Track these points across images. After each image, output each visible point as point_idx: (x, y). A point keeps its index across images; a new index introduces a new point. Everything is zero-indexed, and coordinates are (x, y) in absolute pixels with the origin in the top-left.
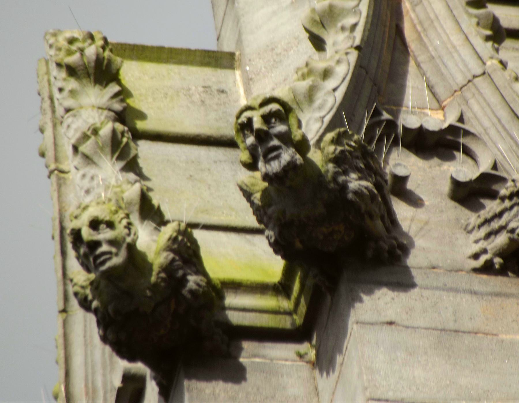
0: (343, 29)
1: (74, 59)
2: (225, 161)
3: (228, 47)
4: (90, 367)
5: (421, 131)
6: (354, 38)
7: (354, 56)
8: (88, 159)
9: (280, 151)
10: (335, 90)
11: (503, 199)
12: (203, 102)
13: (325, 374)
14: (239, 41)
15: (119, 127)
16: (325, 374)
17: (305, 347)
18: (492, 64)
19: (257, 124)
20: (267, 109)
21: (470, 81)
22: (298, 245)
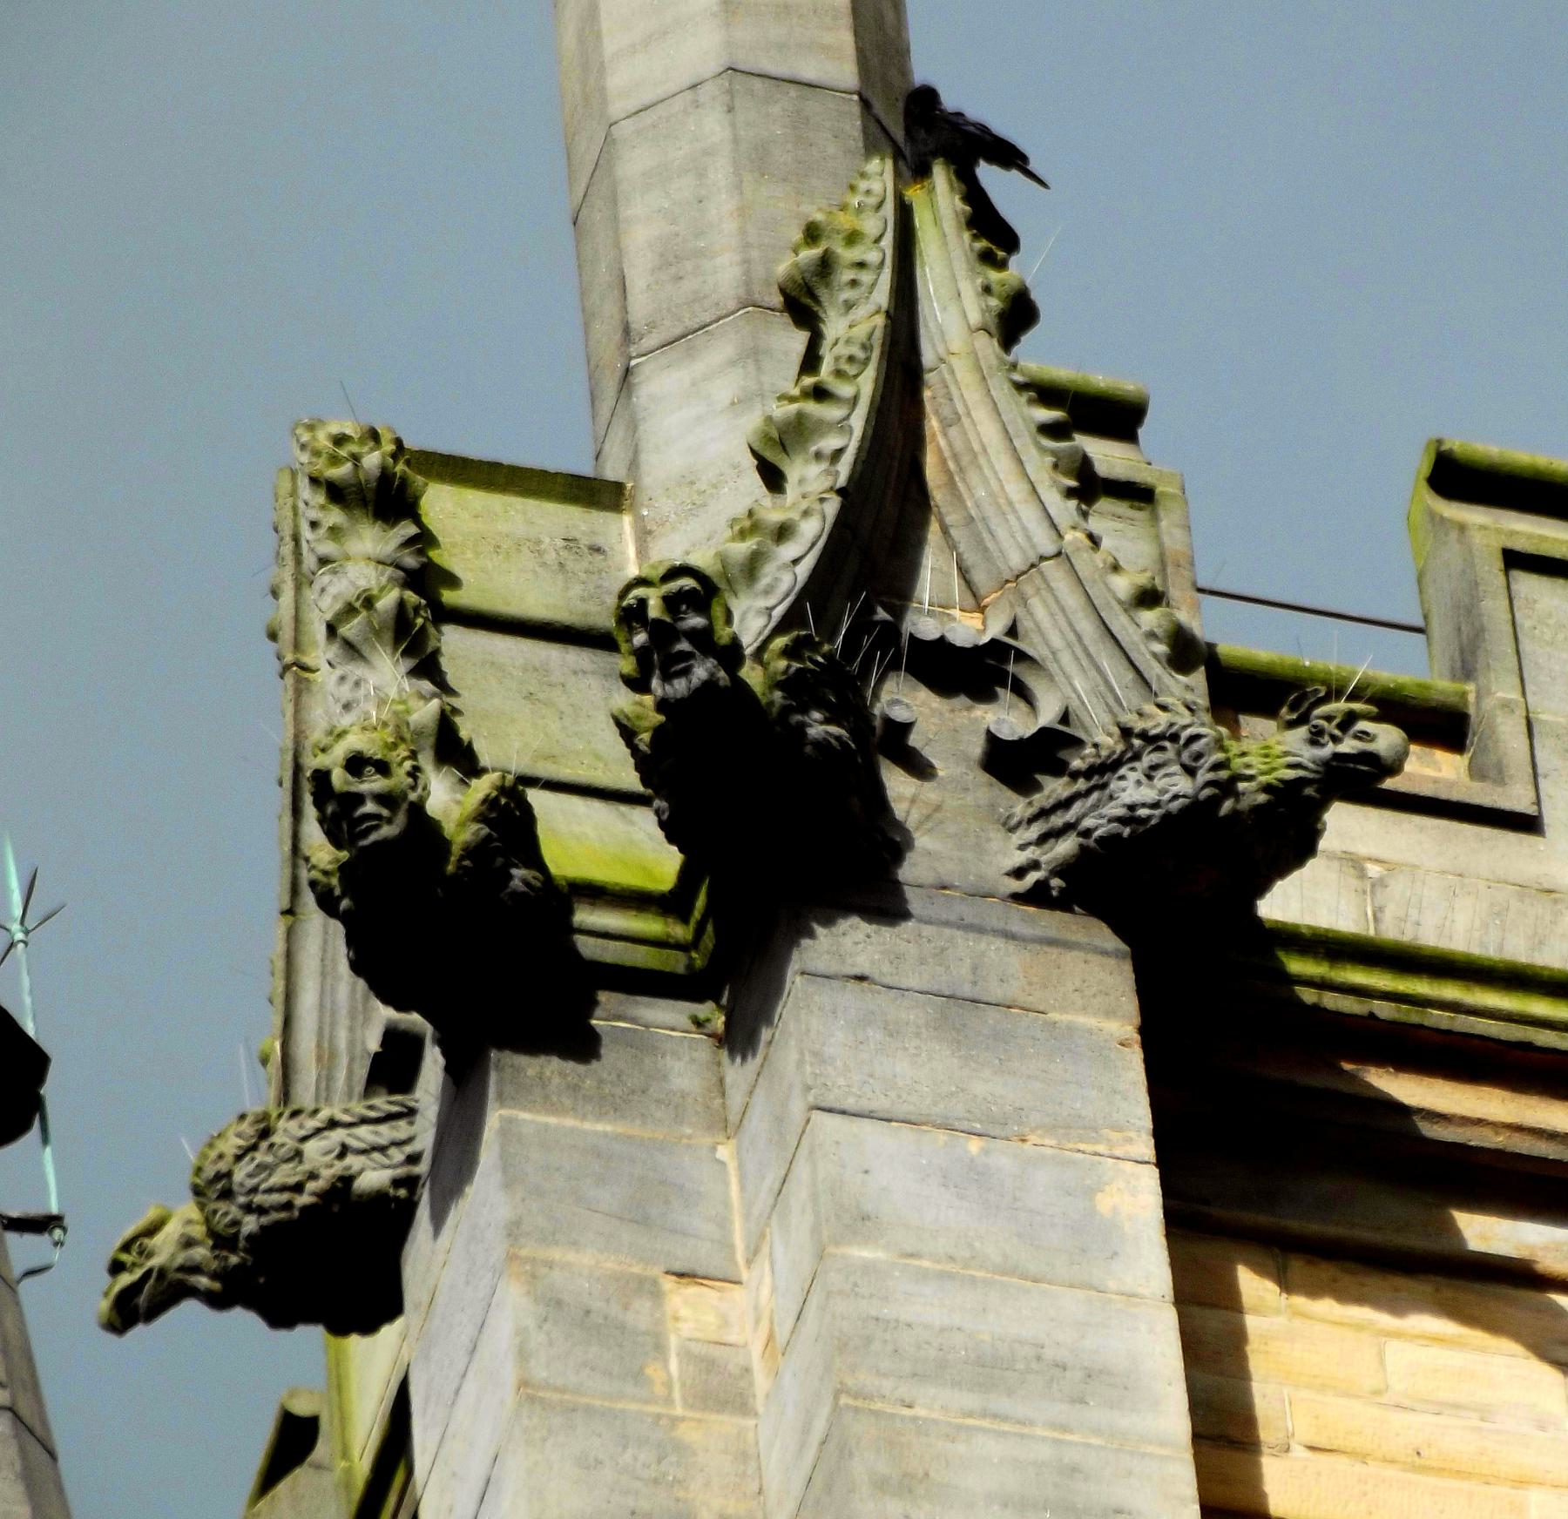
1: (341, 472)
3: (613, 470)
7: (833, 506)
10: (796, 562)
11: (1075, 775)
14: (634, 465)
15: (412, 597)
17: (705, 1009)
19: (655, 610)
21: (1033, 566)
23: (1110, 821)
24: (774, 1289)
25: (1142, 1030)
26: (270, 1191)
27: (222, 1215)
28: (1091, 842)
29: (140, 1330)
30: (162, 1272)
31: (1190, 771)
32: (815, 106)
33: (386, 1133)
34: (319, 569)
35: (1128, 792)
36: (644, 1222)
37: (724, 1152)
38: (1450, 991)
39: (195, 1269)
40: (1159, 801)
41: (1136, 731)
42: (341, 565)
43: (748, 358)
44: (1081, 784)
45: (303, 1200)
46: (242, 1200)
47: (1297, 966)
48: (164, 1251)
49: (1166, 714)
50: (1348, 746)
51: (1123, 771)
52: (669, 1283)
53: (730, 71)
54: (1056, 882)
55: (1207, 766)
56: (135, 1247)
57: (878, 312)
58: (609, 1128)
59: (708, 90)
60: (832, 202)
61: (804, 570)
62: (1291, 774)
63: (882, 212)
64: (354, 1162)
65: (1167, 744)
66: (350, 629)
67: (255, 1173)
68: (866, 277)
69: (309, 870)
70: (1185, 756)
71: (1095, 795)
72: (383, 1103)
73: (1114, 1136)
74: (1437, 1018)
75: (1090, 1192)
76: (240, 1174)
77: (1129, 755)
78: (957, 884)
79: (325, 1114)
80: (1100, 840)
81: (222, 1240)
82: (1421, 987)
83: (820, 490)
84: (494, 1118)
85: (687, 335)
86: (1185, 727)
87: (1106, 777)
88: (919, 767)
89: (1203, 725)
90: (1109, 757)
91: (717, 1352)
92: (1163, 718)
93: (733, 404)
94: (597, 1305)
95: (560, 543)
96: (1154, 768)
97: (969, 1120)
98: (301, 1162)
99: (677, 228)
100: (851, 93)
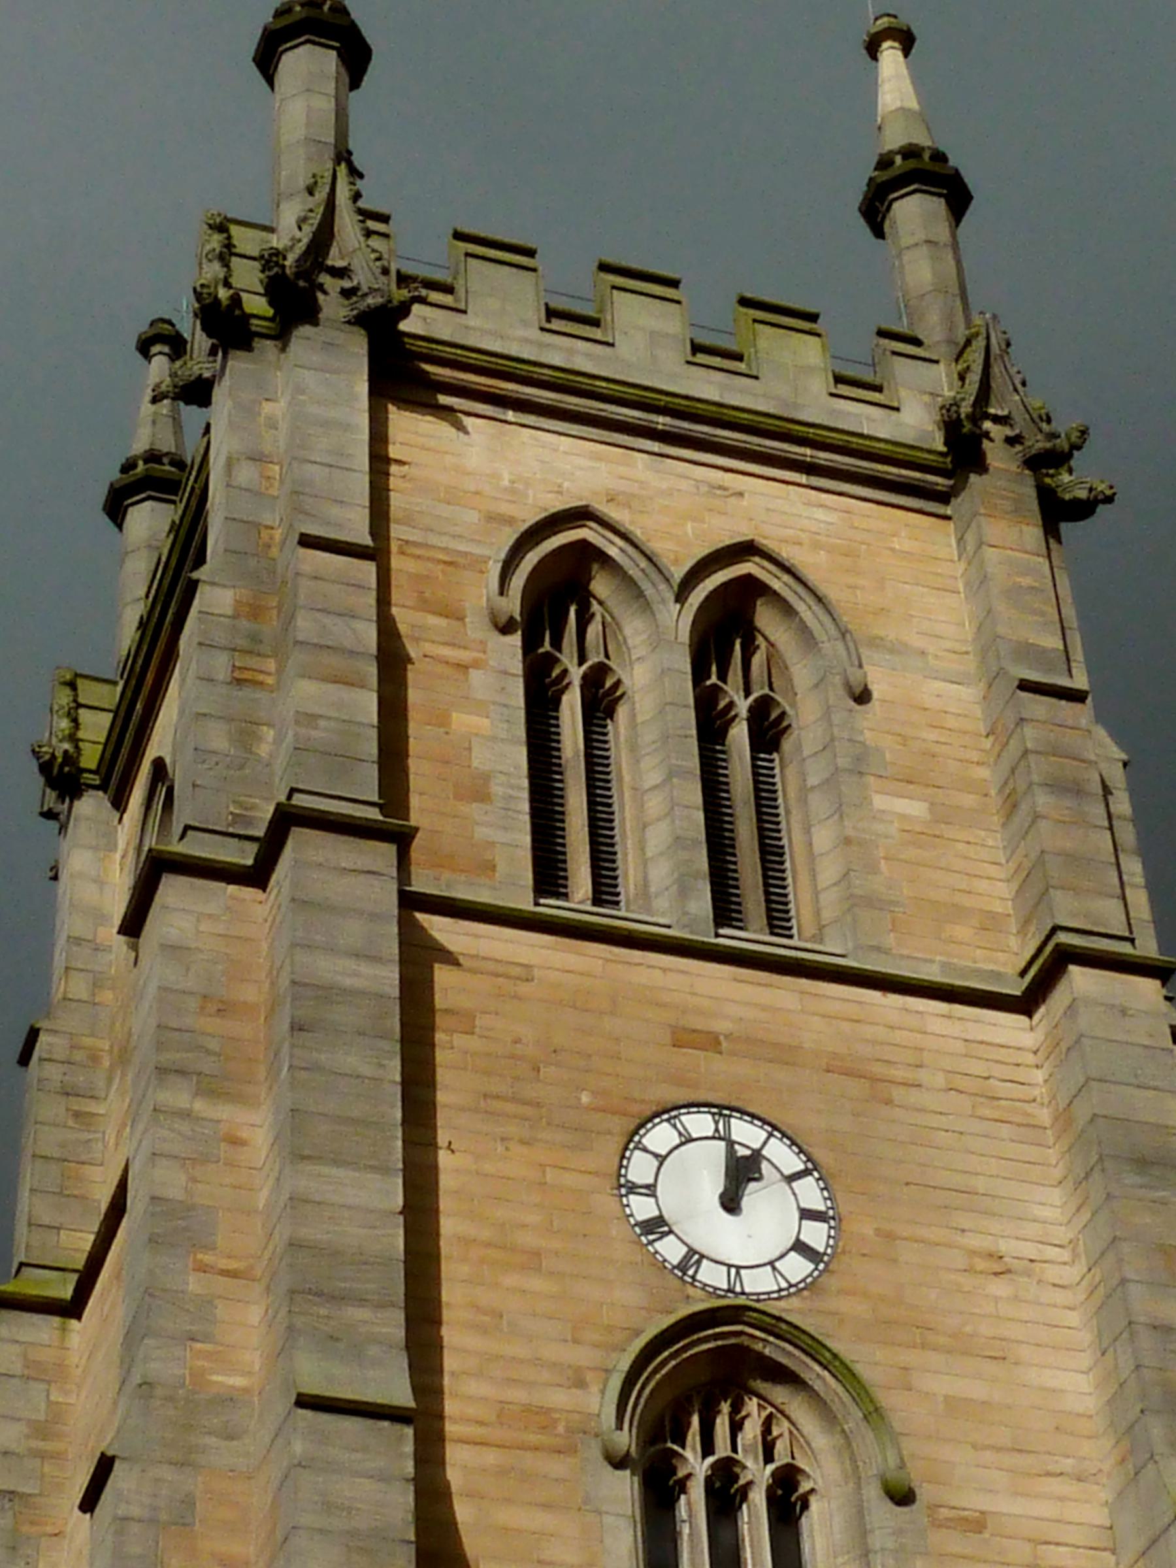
1: (211, 222)
3: (274, 225)
5: (333, 267)
14: (278, 223)
15: (225, 250)
17: (277, 343)
18: (363, 245)
19: (266, 256)
37: (279, 374)
38: (440, 347)
47: (406, 340)
48: (163, 388)
50: (416, 294)
72: (211, 359)
74: (435, 353)
81: (175, 386)
82: (434, 346)
84: (230, 363)
88: (325, 293)
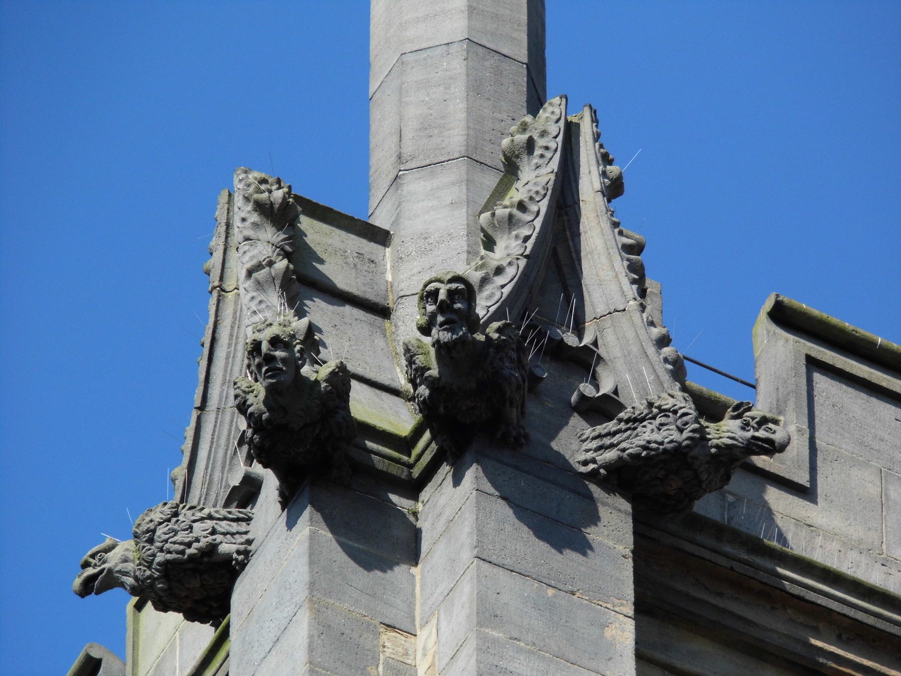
0: (517, 237)
2: (365, 321)
4: (211, 462)
6: (526, 247)
7: (523, 263)
8: (259, 285)
9: (456, 324)
10: (503, 286)
11: (620, 420)
12: (355, 265)
13: (589, 552)
14: (396, 222)
16: (589, 552)
19: (442, 296)
20: (454, 286)
21: (610, 313)
22: (442, 410)
23: (637, 446)
24: (437, 642)
25: (633, 552)
26: (174, 543)
27: (146, 549)
28: (625, 455)
29: (93, 596)
30: (110, 571)
31: (681, 431)
32: (506, 66)
33: (234, 527)
34: (244, 242)
35: (647, 434)
36: (374, 596)
39: (126, 574)
40: (663, 442)
41: (656, 405)
42: (255, 242)
43: (462, 182)
44: (623, 426)
45: (189, 551)
46: (158, 544)
49: (672, 399)
50: (761, 434)
51: (645, 423)
52: (382, 629)
53: (467, 40)
54: (602, 471)
55: (689, 429)
56: (98, 557)
57: (552, 172)
58: (361, 547)
59: (454, 48)
60: (509, 115)
61: (507, 290)
62: (730, 442)
63: (559, 124)
64: (219, 538)
65: (671, 414)
66: (259, 274)
67: (168, 532)
68: (548, 155)
69: (235, 389)
70: (679, 423)
71: (629, 432)
72: (235, 511)
73: (617, 601)
75: (604, 625)
76: (160, 531)
77: (650, 416)
78: (554, 462)
79: (206, 511)
80: (630, 455)
83: (517, 253)
85: (431, 165)
86: (681, 408)
87: (636, 425)
89: (690, 408)
90: (640, 415)
91: (402, 667)
92: (671, 401)
93: (452, 203)
94: (348, 632)
95: (356, 255)
96: (662, 425)
97: (548, 579)
98: (191, 532)
99: (432, 112)
100: (523, 63)
